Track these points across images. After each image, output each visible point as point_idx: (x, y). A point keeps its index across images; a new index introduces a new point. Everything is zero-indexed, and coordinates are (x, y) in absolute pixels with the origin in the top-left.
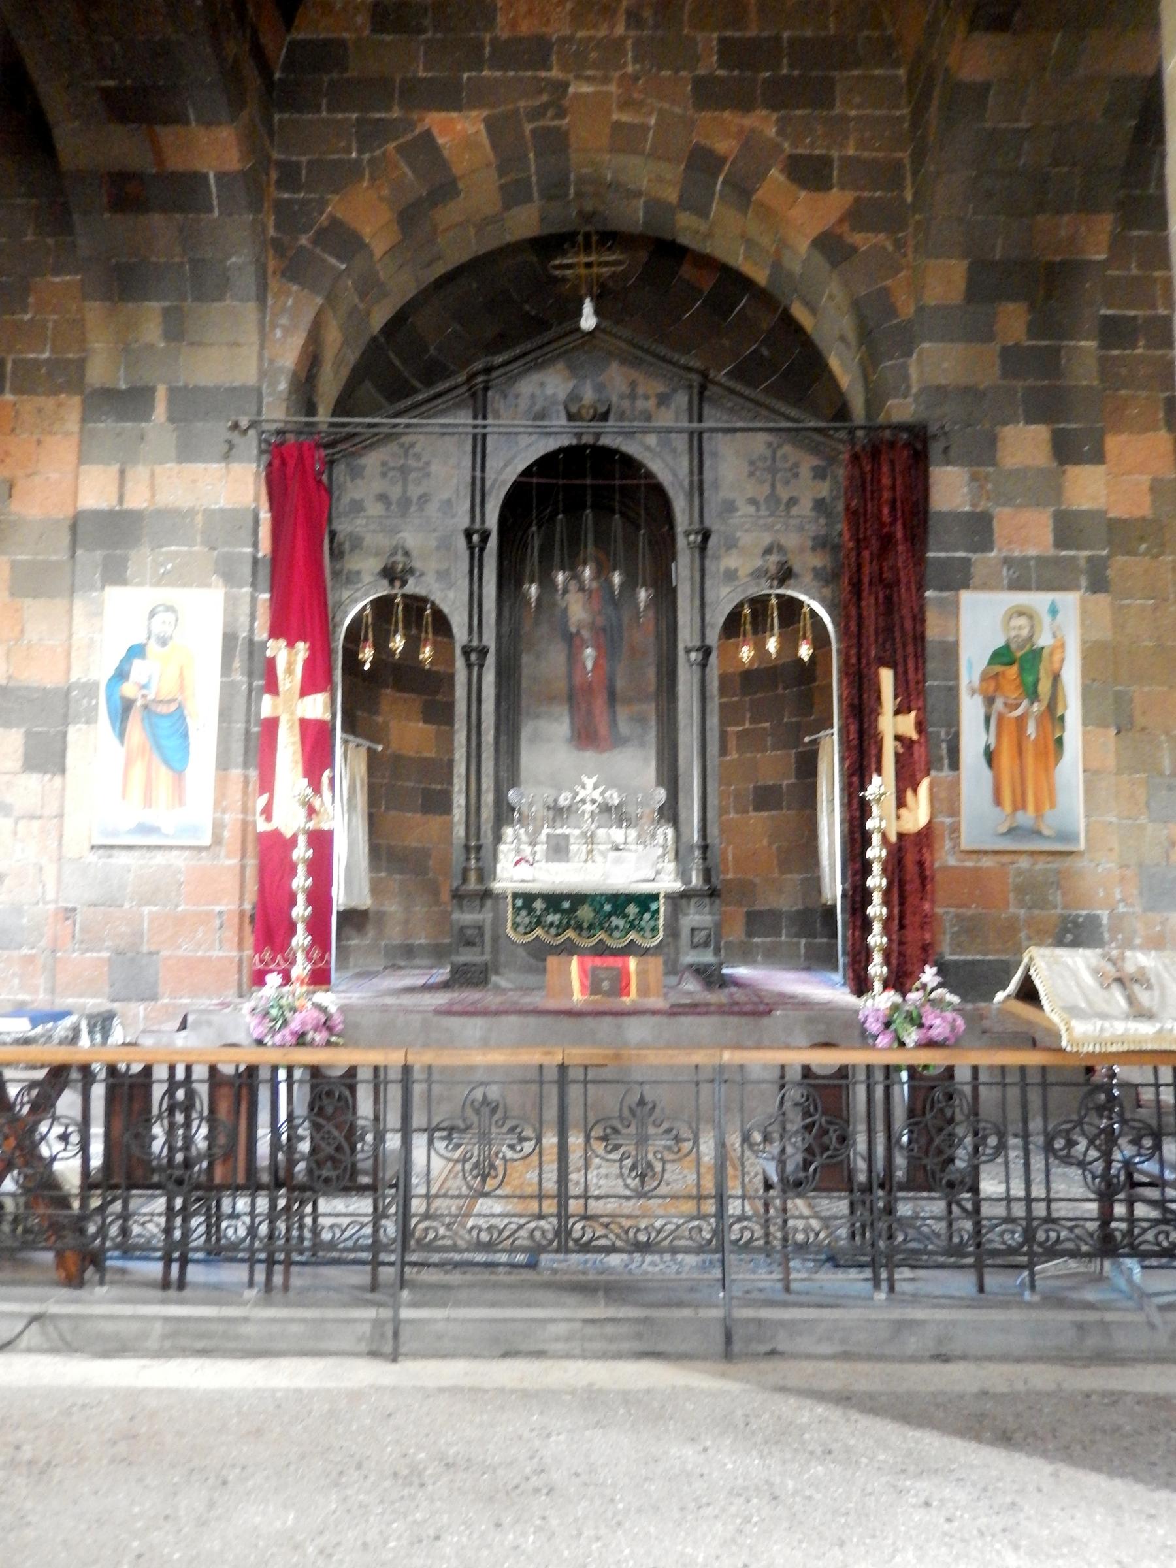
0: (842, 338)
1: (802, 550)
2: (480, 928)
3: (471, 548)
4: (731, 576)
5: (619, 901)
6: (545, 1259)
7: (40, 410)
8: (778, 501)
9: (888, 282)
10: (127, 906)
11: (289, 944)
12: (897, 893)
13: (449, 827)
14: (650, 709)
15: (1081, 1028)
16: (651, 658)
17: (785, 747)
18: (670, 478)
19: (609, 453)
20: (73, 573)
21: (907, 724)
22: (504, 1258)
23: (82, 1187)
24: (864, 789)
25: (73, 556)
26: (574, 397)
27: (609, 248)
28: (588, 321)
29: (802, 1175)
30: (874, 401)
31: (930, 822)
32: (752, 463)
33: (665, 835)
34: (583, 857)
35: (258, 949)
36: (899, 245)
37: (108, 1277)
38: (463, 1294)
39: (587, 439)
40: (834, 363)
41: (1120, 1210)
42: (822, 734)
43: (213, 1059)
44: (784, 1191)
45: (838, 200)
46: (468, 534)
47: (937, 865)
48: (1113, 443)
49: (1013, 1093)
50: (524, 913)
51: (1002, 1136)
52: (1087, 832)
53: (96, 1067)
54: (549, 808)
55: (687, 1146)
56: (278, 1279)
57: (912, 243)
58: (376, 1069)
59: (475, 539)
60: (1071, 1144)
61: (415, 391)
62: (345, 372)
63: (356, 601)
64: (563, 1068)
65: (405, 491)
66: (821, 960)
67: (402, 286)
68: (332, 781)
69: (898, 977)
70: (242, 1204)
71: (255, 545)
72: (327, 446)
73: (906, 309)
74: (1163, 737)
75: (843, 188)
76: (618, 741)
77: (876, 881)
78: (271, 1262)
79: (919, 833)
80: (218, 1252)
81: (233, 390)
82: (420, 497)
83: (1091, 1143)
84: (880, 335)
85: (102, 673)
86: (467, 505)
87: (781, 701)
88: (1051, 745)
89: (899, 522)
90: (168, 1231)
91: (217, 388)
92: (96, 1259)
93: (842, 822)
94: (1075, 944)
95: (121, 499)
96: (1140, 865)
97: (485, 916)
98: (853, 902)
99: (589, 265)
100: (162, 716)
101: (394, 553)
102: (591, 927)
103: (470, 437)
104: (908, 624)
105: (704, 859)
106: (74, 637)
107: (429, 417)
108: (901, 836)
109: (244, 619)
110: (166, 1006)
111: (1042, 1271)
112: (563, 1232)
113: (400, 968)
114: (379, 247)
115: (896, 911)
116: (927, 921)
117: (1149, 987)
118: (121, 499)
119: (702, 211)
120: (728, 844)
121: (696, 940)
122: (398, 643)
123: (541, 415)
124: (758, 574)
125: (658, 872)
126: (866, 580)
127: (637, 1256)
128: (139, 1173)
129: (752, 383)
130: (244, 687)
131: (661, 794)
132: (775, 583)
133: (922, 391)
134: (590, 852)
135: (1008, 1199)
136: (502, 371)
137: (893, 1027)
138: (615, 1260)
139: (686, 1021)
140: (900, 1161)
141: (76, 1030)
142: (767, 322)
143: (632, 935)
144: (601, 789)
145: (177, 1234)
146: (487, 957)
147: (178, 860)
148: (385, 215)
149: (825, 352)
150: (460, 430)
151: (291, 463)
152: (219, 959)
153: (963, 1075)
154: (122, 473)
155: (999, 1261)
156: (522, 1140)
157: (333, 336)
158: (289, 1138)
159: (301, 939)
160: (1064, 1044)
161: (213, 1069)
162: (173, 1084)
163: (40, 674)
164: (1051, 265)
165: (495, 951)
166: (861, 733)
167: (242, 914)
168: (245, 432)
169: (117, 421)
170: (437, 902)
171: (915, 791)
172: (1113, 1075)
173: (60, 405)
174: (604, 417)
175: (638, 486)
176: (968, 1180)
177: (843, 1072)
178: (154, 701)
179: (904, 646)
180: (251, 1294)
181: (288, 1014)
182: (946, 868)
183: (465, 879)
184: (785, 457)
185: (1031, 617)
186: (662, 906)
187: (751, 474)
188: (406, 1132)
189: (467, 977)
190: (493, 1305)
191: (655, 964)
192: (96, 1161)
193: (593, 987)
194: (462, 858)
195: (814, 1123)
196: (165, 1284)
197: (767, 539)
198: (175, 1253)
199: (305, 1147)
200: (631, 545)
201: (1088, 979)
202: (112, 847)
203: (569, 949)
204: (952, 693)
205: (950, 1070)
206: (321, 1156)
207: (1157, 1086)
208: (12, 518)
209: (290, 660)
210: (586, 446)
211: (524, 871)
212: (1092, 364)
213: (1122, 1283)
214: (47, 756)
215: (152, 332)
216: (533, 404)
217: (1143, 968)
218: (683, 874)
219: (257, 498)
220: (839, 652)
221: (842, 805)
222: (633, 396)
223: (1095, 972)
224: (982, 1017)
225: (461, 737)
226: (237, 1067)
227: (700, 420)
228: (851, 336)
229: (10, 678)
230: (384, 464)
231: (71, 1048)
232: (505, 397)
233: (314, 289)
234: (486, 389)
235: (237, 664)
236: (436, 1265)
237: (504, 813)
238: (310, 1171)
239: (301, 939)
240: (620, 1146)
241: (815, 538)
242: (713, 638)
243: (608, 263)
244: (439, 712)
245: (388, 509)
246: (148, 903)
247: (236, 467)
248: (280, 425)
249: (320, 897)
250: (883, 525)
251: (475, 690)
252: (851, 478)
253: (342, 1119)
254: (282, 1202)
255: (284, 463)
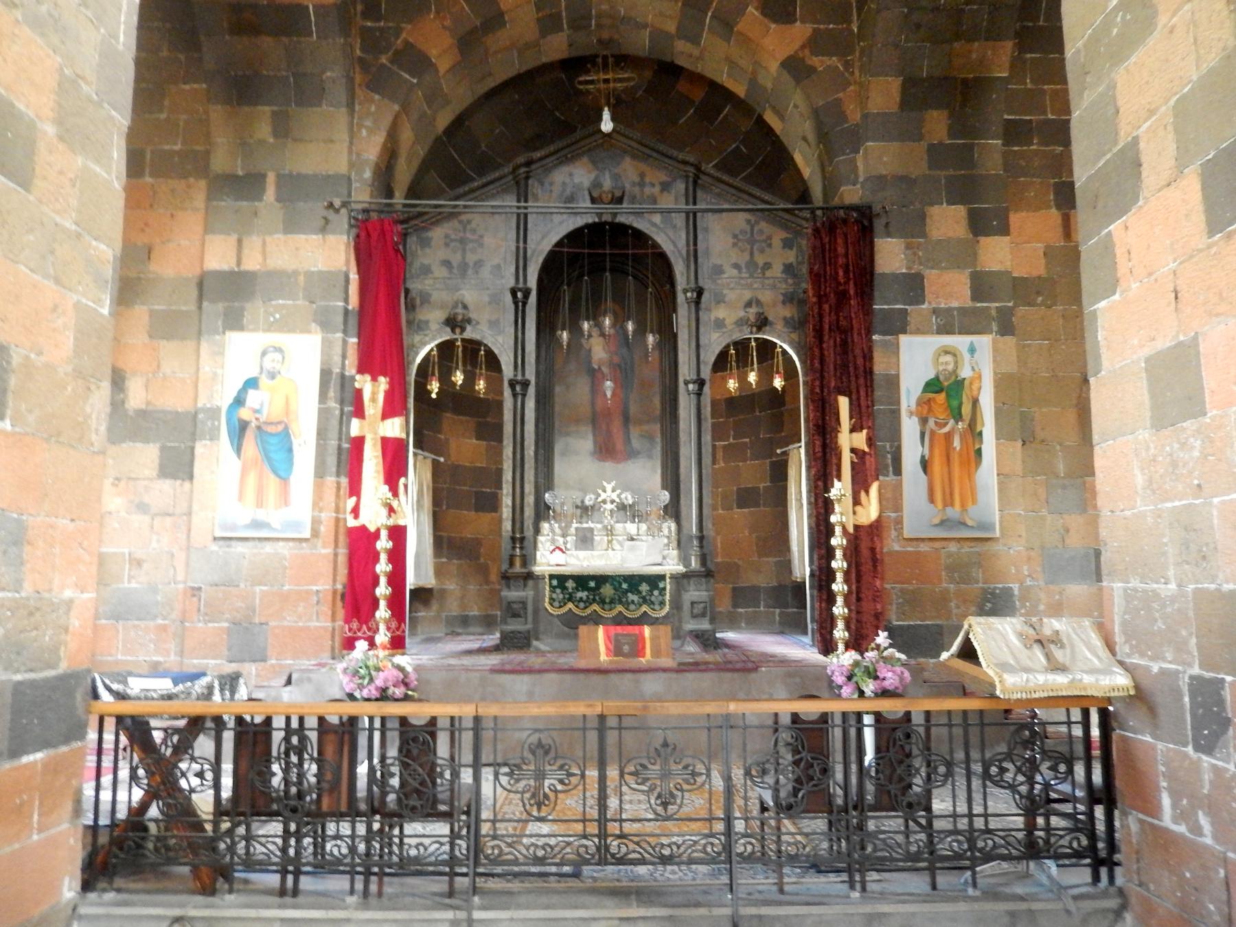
0: (805, 139)
1: (774, 305)
2: (524, 603)
3: (516, 303)
4: (719, 324)
5: (634, 581)
6: (586, 870)
7: (173, 191)
8: (756, 265)
9: (841, 95)
10: (242, 585)
11: (373, 615)
12: (855, 574)
13: (500, 521)
14: (657, 427)
15: (1011, 680)
16: (657, 389)
17: (765, 458)
18: (672, 248)
19: (623, 229)
20: (200, 321)
21: (860, 440)
22: (554, 869)
23: (214, 814)
24: (828, 491)
25: (200, 308)
26: (596, 184)
27: (622, 69)
28: (607, 125)
29: (792, 800)
30: (830, 186)
31: (880, 516)
32: (735, 236)
33: (669, 528)
34: (605, 546)
35: (347, 621)
36: (847, 65)
37: (236, 886)
38: (523, 899)
39: (607, 218)
40: (798, 158)
41: (1040, 821)
42: (791, 447)
43: (321, 711)
44: (778, 813)
45: (800, 31)
46: (513, 292)
47: (885, 550)
48: (1015, 219)
49: (958, 731)
50: (558, 591)
51: (949, 765)
52: (1001, 522)
53: (226, 718)
54: (577, 507)
55: (700, 780)
56: (373, 888)
57: (857, 64)
58: (452, 718)
59: (519, 296)
60: (1003, 770)
61: (473, 180)
62: (416, 164)
63: (425, 344)
64: (602, 718)
65: (464, 258)
66: (793, 625)
67: (460, 95)
68: (406, 486)
69: (856, 640)
70: (345, 828)
71: (346, 300)
72: (402, 222)
73: (854, 115)
74: (1058, 447)
75: (803, 22)
76: (631, 454)
77: (838, 563)
78: (368, 874)
79: (871, 526)
80: (325, 866)
81: (328, 177)
82: (475, 264)
83: (1019, 770)
84: (834, 136)
85: (224, 400)
86: (513, 269)
87: (758, 421)
88: (972, 454)
89: (851, 283)
90: (284, 850)
91: (315, 176)
92: (225, 873)
93: (809, 516)
94: (993, 613)
95: (239, 263)
96: (1042, 548)
97: (528, 593)
98: (820, 580)
99: (606, 81)
100: (271, 435)
101: (455, 306)
102: (612, 602)
103: (515, 216)
104: (860, 361)
105: (701, 547)
106: (201, 371)
107: (483, 200)
108: (856, 527)
109: (337, 359)
110: (272, 665)
111: (982, 871)
112: (603, 849)
113: (458, 634)
114: (443, 65)
115: (854, 587)
116: (878, 596)
117: (1062, 647)
118: (239, 263)
119: (695, 40)
120: (718, 534)
121: (695, 611)
122: (459, 378)
123: (571, 199)
124: (741, 322)
125: (664, 558)
126: (827, 327)
127: (660, 868)
128: (261, 802)
129: (733, 173)
130: (337, 412)
131: (665, 496)
132: (755, 329)
133: (867, 179)
134: (610, 542)
135: (955, 816)
136: (538, 164)
137: (855, 679)
138: (642, 870)
139: (690, 676)
140: (870, 787)
141: (210, 688)
142: (746, 125)
143: (644, 608)
144: (618, 491)
145: (292, 852)
146: (529, 626)
147: (284, 549)
148: (447, 40)
149: (790, 149)
150: (508, 210)
151: (375, 235)
152: (316, 628)
153: (918, 719)
154: (240, 242)
155: (946, 865)
156: (570, 775)
157: (407, 135)
158: (382, 774)
159: (383, 613)
160: (998, 693)
161: (321, 720)
162: (288, 730)
163: (174, 401)
164: (965, 82)
165: (536, 621)
166: (824, 446)
167: (335, 592)
168: (337, 211)
169: (236, 200)
170: (487, 582)
171: (867, 492)
172: (1034, 716)
173: (189, 186)
174: (620, 200)
175: (646, 255)
176: (923, 802)
177: (824, 718)
178: (265, 423)
179: (857, 377)
180: (352, 900)
181: (373, 673)
182: (890, 553)
183: (512, 564)
184: (761, 232)
185: (955, 355)
186: (668, 585)
187: (735, 245)
188: (477, 766)
189: (514, 642)
190: (547, 907)
191: (665, 631)
192: (226, 794)
193: (617, 651)
194: (509, 547)
195: (801, 759)
196: (282, 892)
197: (747, 295)
198: (290, 867)
199: (395, 782)
200: (641, 301)
201: (1015, 641)
202: (230, 539)
203: (596, 620)
204: (896, 414)
205: (908, 715)
206: (408, 789)
207: (1069, 723)
208: (151, 276)
209: (374, 390)
210: (606, 223)
211: (558, 557)
212: (997, 159)
213: (1044, 880)
214: (178, 465)
215: (264, 130)
216: (564, 190)
217: (1057, 632)
218: (684, 560)
219: (347, 262)
220: (805, 383)
221: (809, 503)
222: (642, 184)
223: (1020, 635)
224: (923, 669)
225: (508, 451)
226: (341, 718)
227: (695, 203)
228: (811, 137)
229: (148, 403)
230: (447, 236)
231: (206, 703)
232: (542, 184)
233: (393, 98)
234: (527, 178)
235: (331, 394)
236: (499, 875)
237: (543, 511)
238: (399, 800)
239: (383, 613)
240: (648, 779)
241: (784, 295)
242: (706, 373)
243: (621, 80)
244: (490, 431)
245: (451, 272)
246: (260, 584)
247: (331, 238)
248: (366, 205)
249: (397, 578)
250: (839, 284)
251: (519, 415)
252: (814, 248)
253: (424, 759)
254: (376, 826)
255: (368, 235)
